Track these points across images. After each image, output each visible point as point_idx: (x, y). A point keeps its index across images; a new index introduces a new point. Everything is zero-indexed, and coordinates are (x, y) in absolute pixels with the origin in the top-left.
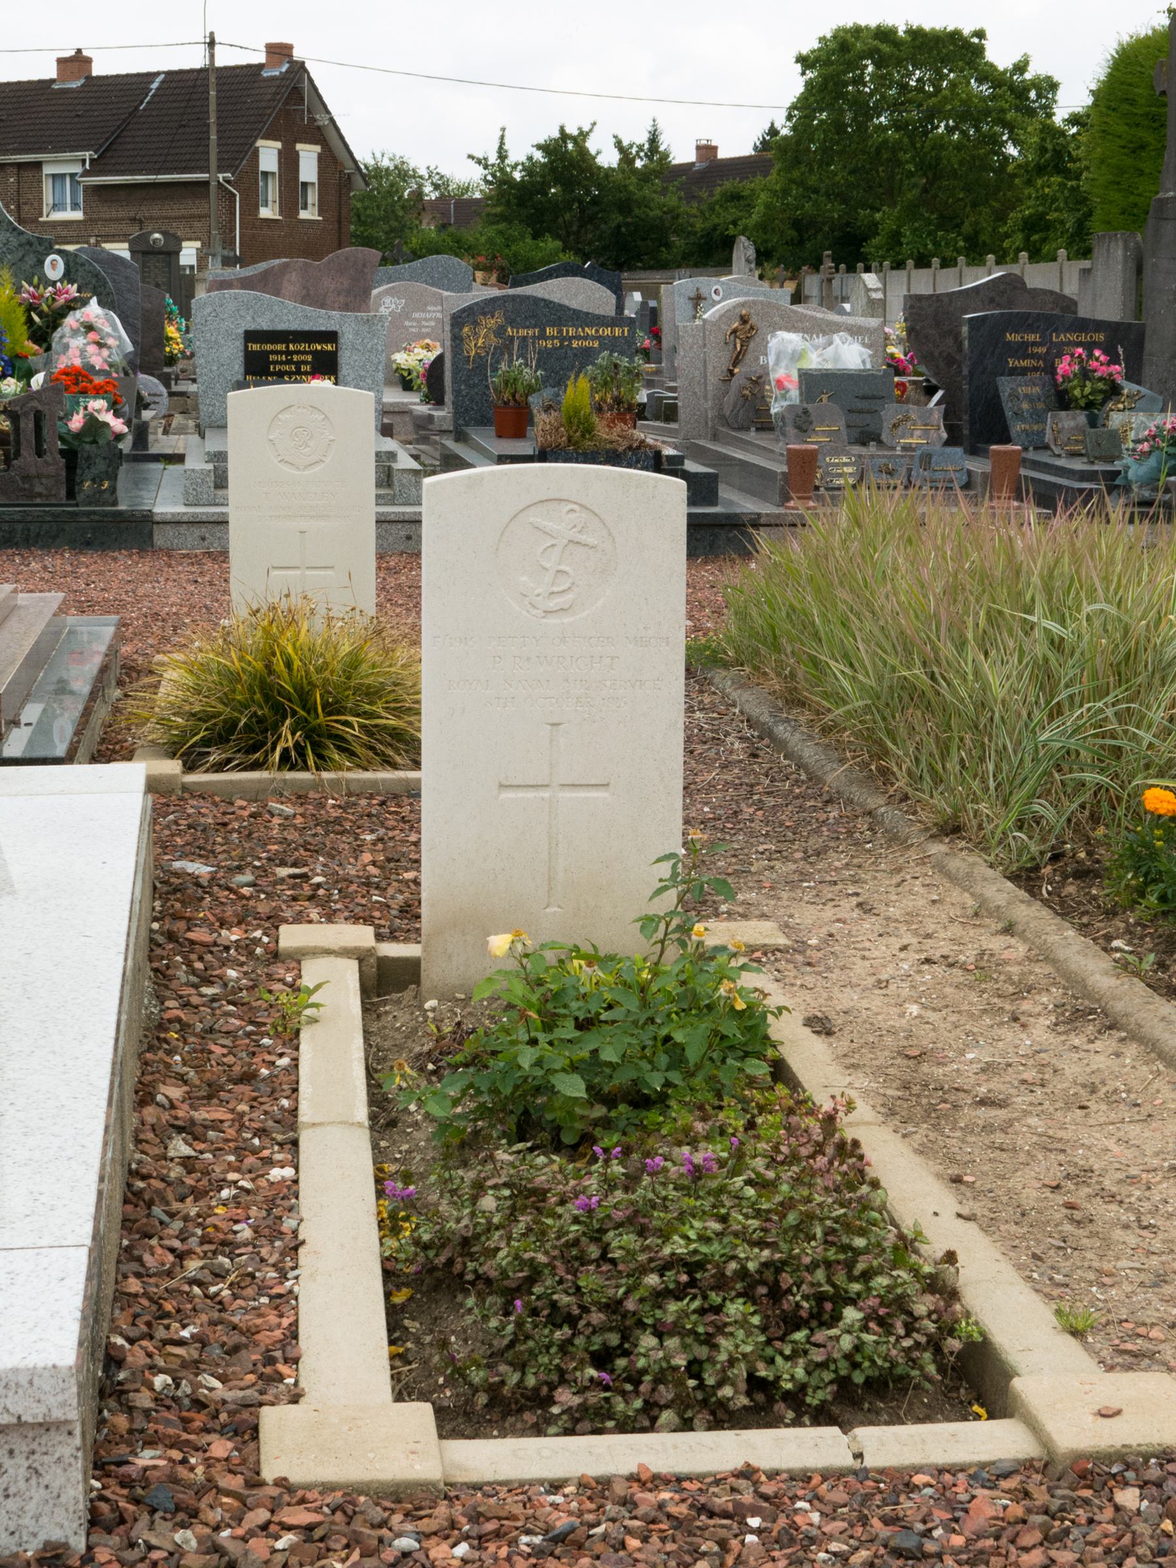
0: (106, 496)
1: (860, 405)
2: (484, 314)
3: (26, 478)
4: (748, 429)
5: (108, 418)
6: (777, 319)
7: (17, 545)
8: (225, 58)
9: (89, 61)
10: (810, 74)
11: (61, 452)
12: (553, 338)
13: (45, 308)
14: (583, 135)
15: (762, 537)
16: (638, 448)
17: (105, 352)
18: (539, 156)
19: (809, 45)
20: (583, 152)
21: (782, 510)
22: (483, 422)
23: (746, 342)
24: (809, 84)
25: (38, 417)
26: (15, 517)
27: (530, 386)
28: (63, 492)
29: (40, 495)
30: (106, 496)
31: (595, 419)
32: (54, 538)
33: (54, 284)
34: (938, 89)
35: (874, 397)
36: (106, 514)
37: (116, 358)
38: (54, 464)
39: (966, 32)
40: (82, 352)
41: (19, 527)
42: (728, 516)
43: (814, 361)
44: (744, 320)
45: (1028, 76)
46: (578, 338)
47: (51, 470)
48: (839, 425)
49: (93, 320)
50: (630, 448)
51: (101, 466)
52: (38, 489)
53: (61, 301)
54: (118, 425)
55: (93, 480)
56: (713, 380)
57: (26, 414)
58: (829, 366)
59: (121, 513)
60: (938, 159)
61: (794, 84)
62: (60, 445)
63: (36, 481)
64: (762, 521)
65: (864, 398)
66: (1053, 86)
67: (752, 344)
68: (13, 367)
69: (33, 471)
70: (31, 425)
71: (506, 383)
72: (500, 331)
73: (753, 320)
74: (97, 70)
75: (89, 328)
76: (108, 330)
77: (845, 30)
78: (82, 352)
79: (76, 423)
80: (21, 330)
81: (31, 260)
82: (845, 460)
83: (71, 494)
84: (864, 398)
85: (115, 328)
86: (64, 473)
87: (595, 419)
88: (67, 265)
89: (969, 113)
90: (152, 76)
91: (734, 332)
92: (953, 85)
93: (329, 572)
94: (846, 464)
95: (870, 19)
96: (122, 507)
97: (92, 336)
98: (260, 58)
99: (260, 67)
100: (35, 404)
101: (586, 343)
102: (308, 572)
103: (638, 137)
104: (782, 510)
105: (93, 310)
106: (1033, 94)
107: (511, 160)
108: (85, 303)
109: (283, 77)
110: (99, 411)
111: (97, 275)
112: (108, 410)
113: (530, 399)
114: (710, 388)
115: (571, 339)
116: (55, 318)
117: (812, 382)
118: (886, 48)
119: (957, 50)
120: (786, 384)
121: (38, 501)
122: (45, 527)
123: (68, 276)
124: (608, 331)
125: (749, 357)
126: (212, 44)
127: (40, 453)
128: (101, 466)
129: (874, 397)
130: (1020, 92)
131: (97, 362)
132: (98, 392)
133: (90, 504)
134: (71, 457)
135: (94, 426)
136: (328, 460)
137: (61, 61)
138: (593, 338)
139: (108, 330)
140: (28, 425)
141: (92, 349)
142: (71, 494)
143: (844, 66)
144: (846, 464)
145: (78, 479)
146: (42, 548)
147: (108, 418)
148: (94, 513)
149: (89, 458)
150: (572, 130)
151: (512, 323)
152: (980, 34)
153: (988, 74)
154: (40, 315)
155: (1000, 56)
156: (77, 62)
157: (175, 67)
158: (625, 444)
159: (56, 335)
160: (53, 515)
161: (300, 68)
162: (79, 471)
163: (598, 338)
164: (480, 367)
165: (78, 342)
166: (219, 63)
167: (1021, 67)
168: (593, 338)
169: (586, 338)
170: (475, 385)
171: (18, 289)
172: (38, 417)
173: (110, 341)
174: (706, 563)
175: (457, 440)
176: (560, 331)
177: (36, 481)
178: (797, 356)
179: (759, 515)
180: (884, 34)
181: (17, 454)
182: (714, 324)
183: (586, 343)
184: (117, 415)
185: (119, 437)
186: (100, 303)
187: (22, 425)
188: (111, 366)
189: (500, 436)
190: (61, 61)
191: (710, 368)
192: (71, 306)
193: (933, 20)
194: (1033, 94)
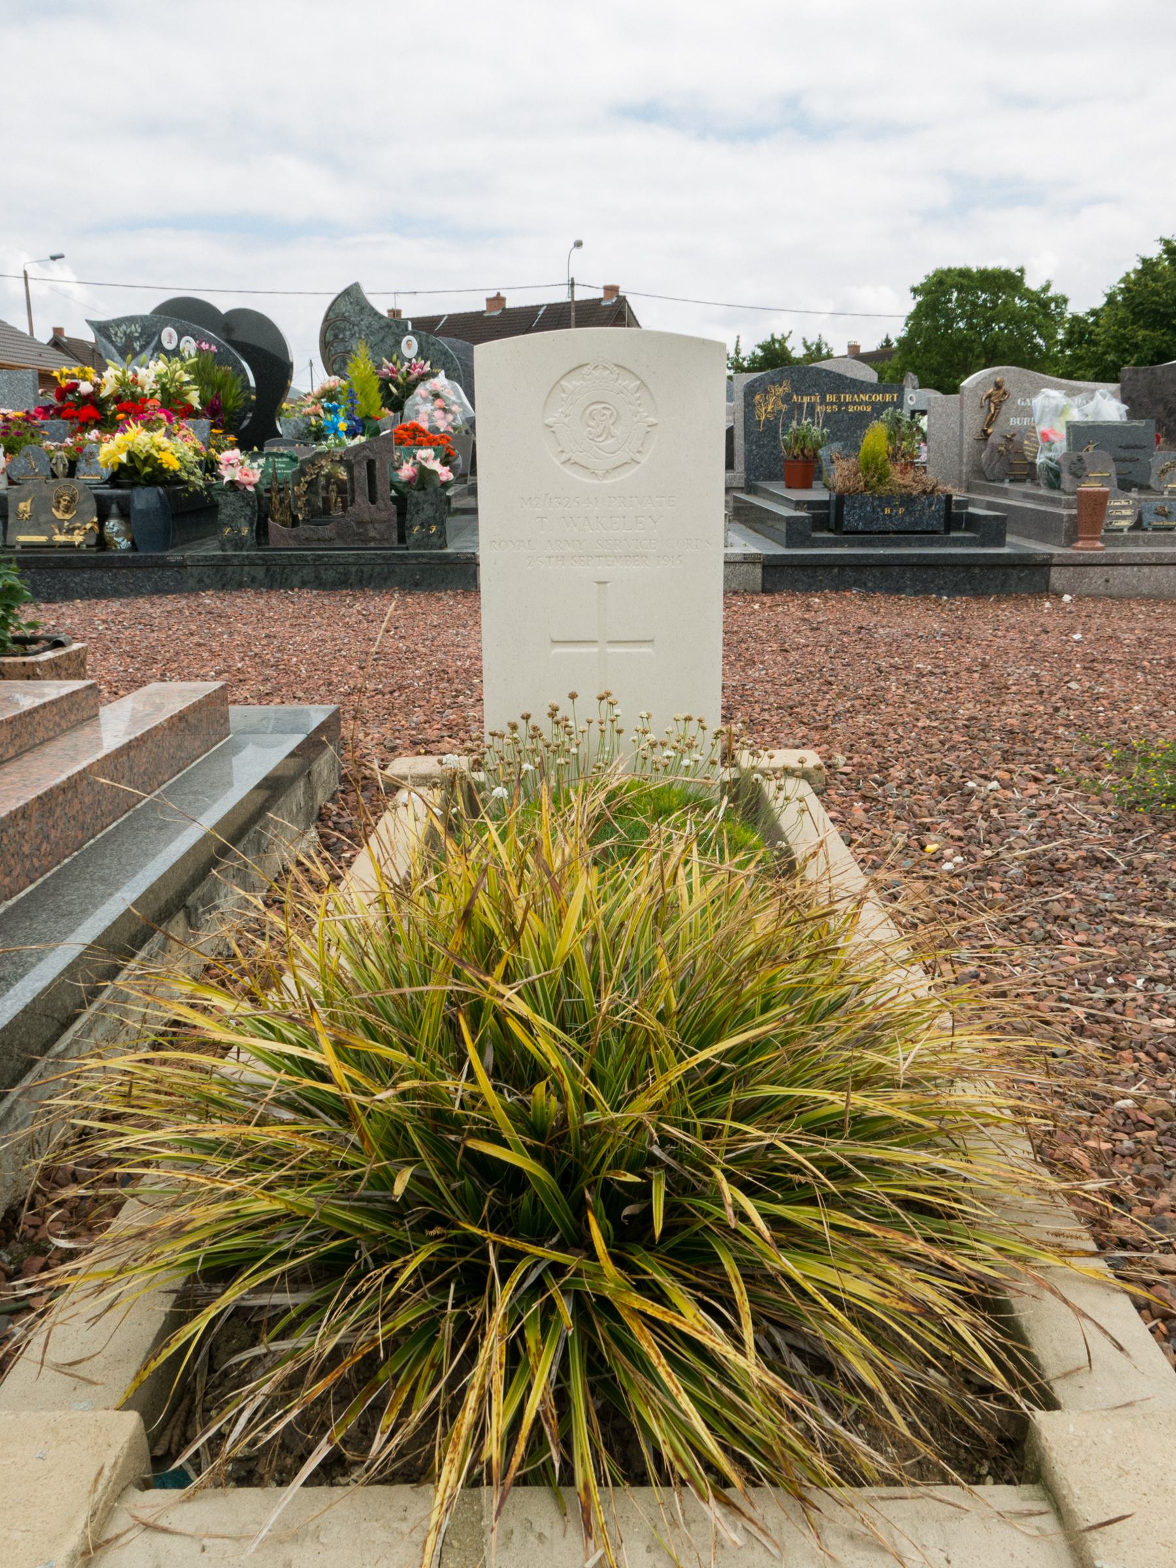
0: (434, 539)
1: (1123, 454)
2: (774, 383)
3: (360, 523)
4: (1002, 481)
5: (435, 465)
6: (1027, 385)
7: (351, 587)
8: (581, 295)
9: (504, 300)
10: (919, 299)
11: (393, 499)
12: (832, 404)
13: (400, 380)
14: (785, 339)
15: (1057, 577)
16: (932, 492)
17: (450, 417)
18: (759, 353)
19: (919, 280)
20: (784, 348)
21: (1069, 551)
22: (771, 477)
23: (998, 406)
24: (919, 305)
25: (371, 465)
26: (351, 560)
27: (817, 442)
28: (395, 537)
29: (374, 539)
30: (434, 539)
31: (889, 466)
32: (386, 579)
33: (410, 360)
34: (995, 305)
35: (1135, 447)
36: (433, 557)
37: (459, 422)
38: (386, 511)
39: (1013, 270)
40: (430, 416)
41: (353, 569)
42: (1021, 556)
43: (1075, 416)
44: (998, 386)
45: (1049, 294)
46: (854, 403)
47: (383, 515)
48: (1111, 471)
49: (439, 389)
50: (924, 492)
51: (428, 511)
52: (372, 533)
53: (415, 375)
54: (445, 474)
55: (422, 525)
56: (968, 439)
57: (359, 463)
58: (1090, 419)
59: (447, 556)
60: (995, 347)
61: (910, 305)
62: (393, 493)
63: (369, 526)
64: (1055, 561)
65: (1127, 447)
66: (1065, 301)
67: (1004, 408)
68: (364, 426)
69: (366, 517)
70: (365, 473)
71: (796, 439)
72: (787, 398)
73: (1006, 387)
74: (509, 305)
75: (437, 396)
76: (454, 398)
77: (943, 272)
78: (430, 416)
79: (406, 471)
80: (376, 398)
81: (390, 341)
82: (1124, 503)
83: (402, 539)
84: (1127, 447)
85: (459, 397)
86: (395, 519)
87: (889, 466)
88: (420, 344)
89: (1015, 318)
90: (539, 307)
91: (989, 396)
92: (1005, 303)
93: (646, 649)
94: (1124, 507)
95: (958, 264)
96: (449, 550)
97: (438, 402)
98: (600, 294)
99: (601, 300)
100: (366, 453)
101: (860, 408)
102: (611, 650)
103: (812, 340)
104: (1069, 551)
105: (441, 381)
106: (1053, 306)
107: (742, 355)
108: (435, 375)
109: (613, 305)
110: (426, 460)
111: (446, 353)
112: (435, 458)
113: (820, 452)
114: (965, 446)
115: (847, 404)
116: (409, 389)
117: (1079, 434)
118: (965, 282)
119: (1006, 282)
120: (1052, 437)
121: (372, 545)
122: (378, 569)
123: (421, 353)
124: (880, 398)
125: (1001, 419)
126: (573, 285)
127: (373, 500)
128: (428, 511)
129: (1135, 447)
130: (1045, 305)
131: (442, 425)
132: (431, 443)
133: (418, 547)
134: (401, 502)
135: (424, 476)
136: (644, 460)
137: (489, 300)
138: (867, 404)
139: (454, 398)
140: (362, 473)
141: (438, 414)
142: (402, 539)
143: (937, 292)
144: (1124, 507)
145: (407, 524)
146: (374, 589)
147: (435, 465)
148: (422, 555)
149: (417, 503)
150: (778, 336)
151: (798, 391)
152: (1022, 271)
153: (1027, 295)
154: (397, 387)
155: (1033, 283)
156: (498, 300)
157: (552, 301)
158: (920, 488)
159: (409, 403)
160: (384, 558)
161: (622, 301)
162: (408, 517)
163: (872, 403)
164: (771, 429)
165: (426, 408)
166: (577, 298)
167: (1046, 289)
168: (867, 404)
169: (860, 404)
170: (764, 446)
171: (379, 366)
172: (371, 465)
173: (455, 408)
174: (998, 601)
175: (748, 493)
176: (839, 398)
177: (369, 526)
178: (1060, 411)
179: (1051, 555)
180: (964, 274)
181: (353, 501)
182: (971, 390)
183: (860, 408)
184: (444, 463)
185: (446, 485)
186: (447, 376)
187: (356, 473)
188: (455, 428)
189: (789, 487)
190: (489, 300)
191: (966, 430)
192: (424, 377)
193: (991, 264)
194: (1053, 306)
